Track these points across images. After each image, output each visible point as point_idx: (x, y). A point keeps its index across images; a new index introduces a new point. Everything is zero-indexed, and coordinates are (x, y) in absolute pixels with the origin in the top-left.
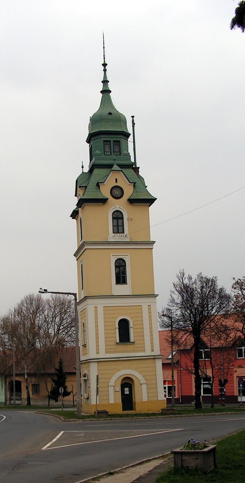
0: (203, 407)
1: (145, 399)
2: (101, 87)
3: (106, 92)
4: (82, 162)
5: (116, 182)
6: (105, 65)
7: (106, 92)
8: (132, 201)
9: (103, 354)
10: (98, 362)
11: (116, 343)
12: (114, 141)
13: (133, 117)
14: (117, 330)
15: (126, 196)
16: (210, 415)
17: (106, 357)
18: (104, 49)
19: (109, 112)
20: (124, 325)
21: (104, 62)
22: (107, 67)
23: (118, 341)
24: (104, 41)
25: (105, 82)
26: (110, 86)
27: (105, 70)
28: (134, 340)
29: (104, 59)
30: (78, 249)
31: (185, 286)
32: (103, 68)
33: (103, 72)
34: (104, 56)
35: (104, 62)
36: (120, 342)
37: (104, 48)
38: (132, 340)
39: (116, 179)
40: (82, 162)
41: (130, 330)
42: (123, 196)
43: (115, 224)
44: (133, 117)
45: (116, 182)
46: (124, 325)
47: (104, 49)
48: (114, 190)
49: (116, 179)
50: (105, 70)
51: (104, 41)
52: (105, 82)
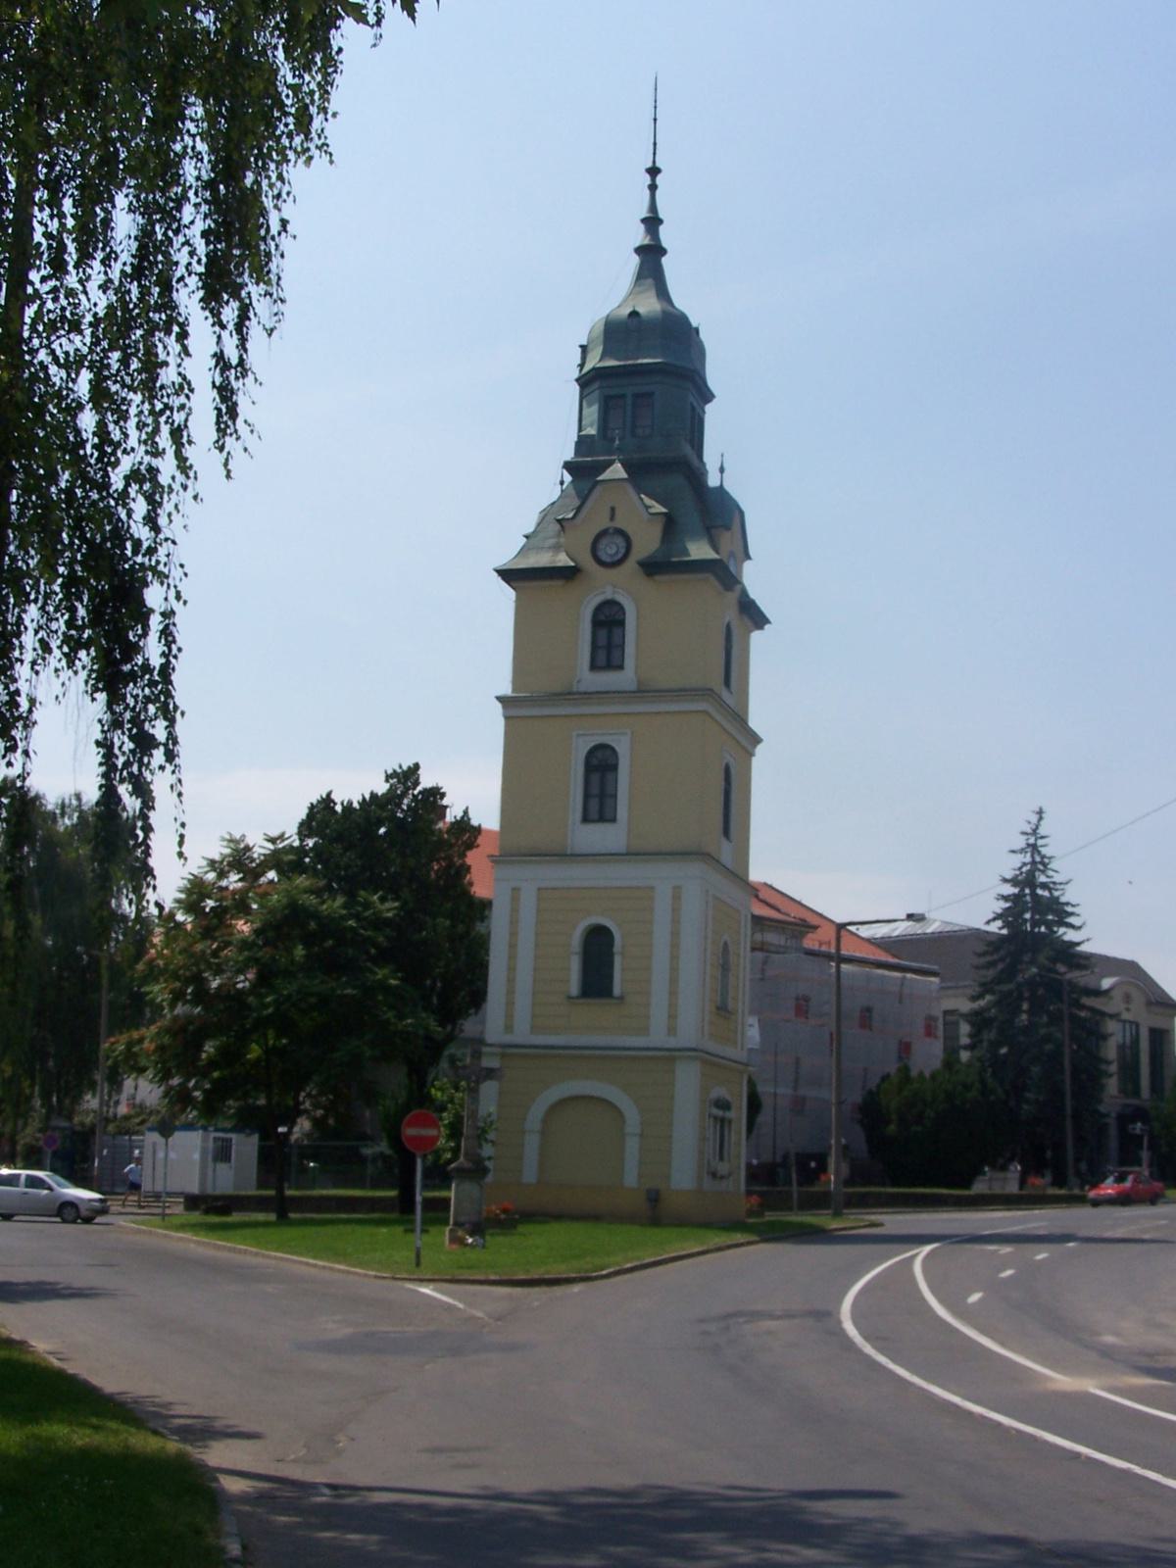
0: (182, 1200)
1: (530, 1175)
2: (640, 236)
3: (651, 255)
4: (722, 455)
6: (654, 171)
7: (651, 255)
9: (522, 1034)
16: (215, 1244)
18: (655, 123)
19: (631, 309)
20: (598, 946)
21: (654, 162)
22: (659, 179)
23: (574, 988)
24: (656, 101)
25: (652, 222)
26: (665, 235)
27: (653, 188)
29: (654, 154)
31: (988, 958)
32: (647, 180)
33: (648, 192)
34: (655, 144)
35: (654, 162)
37: (655, 120)
38: (617, 991)
39: (613, 509)
40: (722, 455)
43: (602, 641)
46: (598, 946)
47: (655, 123)
48: (620, 541)
49: (613, 509)
50: (653, 188)
51: (656, 101)
52: (652, 222)
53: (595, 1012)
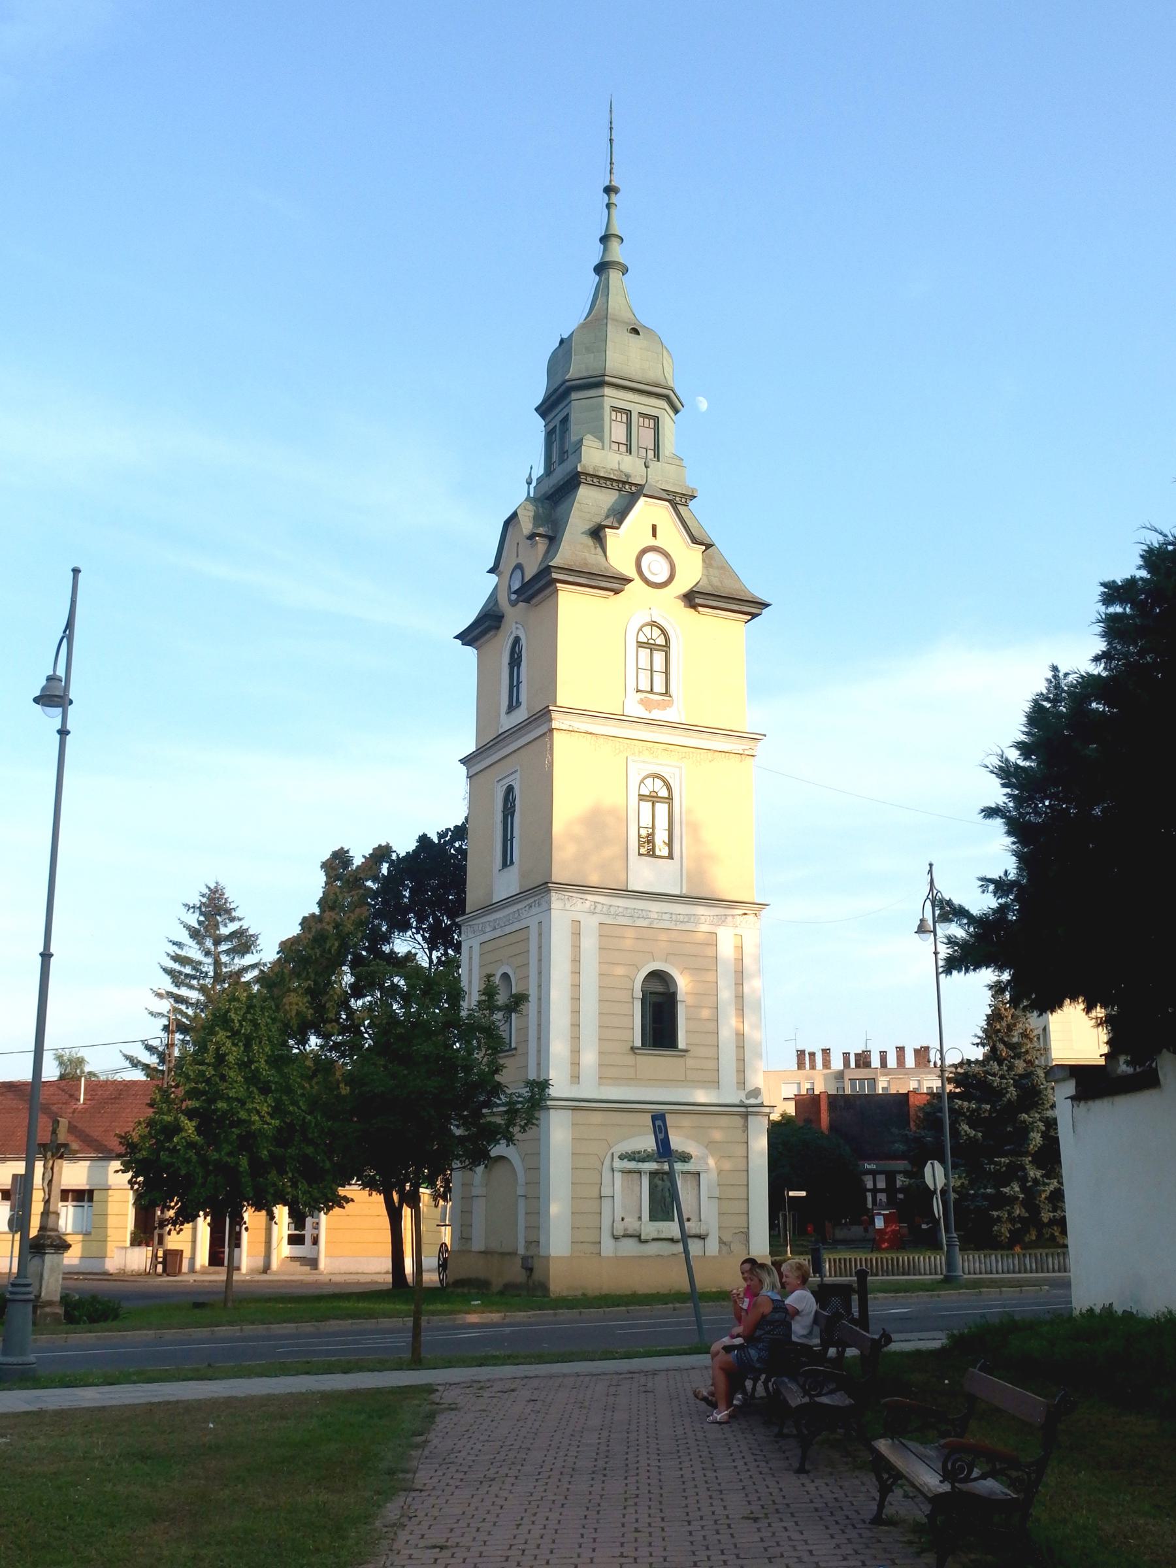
4: (531, 468)
5: (654, 535)
8: (691, 599)
9: (589, 1090)
10: (575, 1109)
11: (632, 1048)
12: (641, 414)
13: (76, 571)
14: (638, 1006)
15: (683, 583)
17: (604, 1097)
23: (638, 1043)
24: (611, 123)
28: (687, 1044)
30: (477, 750)
36: (642, 1046)
38: (682, 1044)
39: (654, 527)
40: (531, 468)
41: (69, 1266)
42: (648, 585)
44: (76, 571)
45: (654, 535)
49: (654, 527)
53: (658, 1062)
